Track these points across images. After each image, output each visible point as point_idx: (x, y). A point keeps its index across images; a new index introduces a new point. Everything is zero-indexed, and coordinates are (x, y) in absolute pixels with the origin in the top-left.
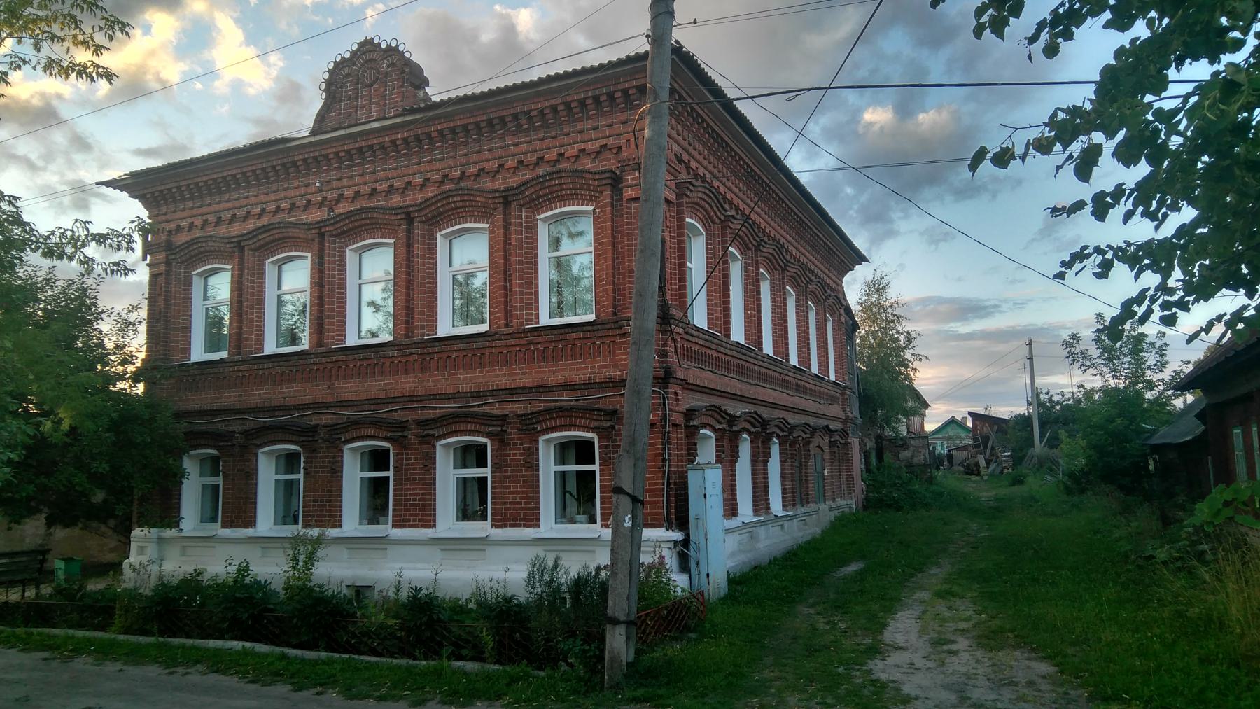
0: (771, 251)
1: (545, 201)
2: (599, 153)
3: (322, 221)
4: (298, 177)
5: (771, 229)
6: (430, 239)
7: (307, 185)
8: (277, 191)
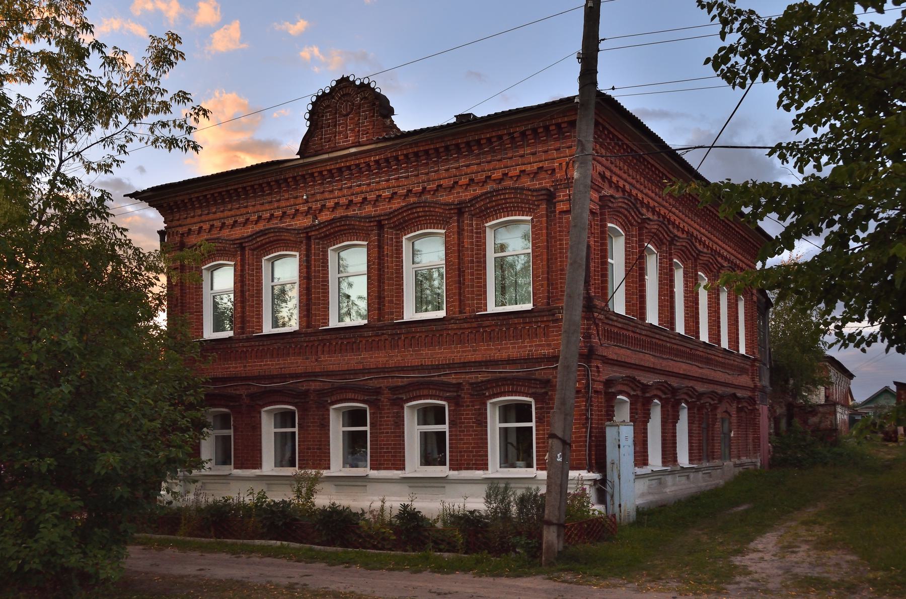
0: (684, 244)
1: (491, 212)
2: (536, 173)
3: (310, 227)
4: (287, 191)
5: (685, 224)
6: (397, 242)
7: (296, 198)
8: (271, 202)
